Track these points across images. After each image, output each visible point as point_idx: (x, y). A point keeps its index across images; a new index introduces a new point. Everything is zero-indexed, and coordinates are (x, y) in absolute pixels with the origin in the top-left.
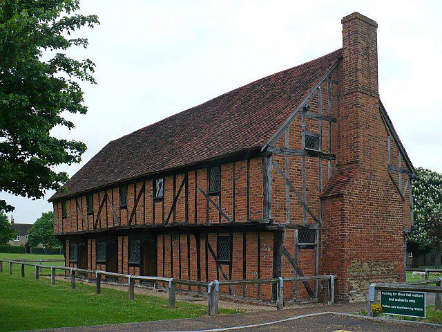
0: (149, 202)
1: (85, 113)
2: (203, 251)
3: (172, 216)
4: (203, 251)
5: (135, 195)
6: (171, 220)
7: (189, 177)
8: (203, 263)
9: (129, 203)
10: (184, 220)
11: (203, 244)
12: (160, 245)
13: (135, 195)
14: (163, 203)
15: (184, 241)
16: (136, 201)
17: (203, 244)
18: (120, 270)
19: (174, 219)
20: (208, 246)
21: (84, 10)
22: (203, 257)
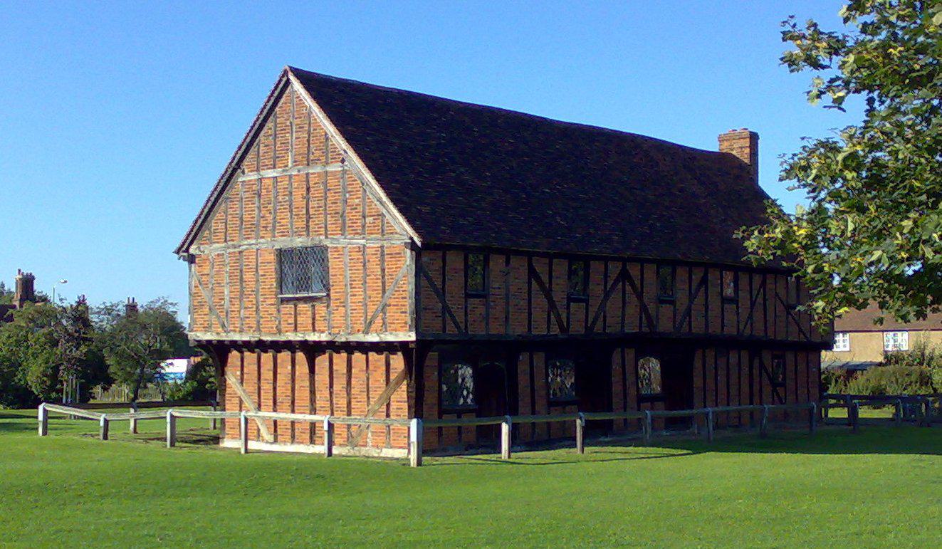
0: (715, 303)
1: (33, 278)
2: (756, 372)
3: (748, 326)
4: (756, 372)
5: (690, 286)
6: (685, 328)
7: (768, 281)
8: (756, 387)
9: (679, 295)
10: (762, 334)
11: (756, 363)
12: (698, 364)
13: (690, 286)
14: (738, 307)
15: (733, 358)
16: (692, 297)
17: (756, 363)
18: (616, 401)
19: (752, 330)
20: (762, 366)
21: (11, 285)
22: (756, 379)
